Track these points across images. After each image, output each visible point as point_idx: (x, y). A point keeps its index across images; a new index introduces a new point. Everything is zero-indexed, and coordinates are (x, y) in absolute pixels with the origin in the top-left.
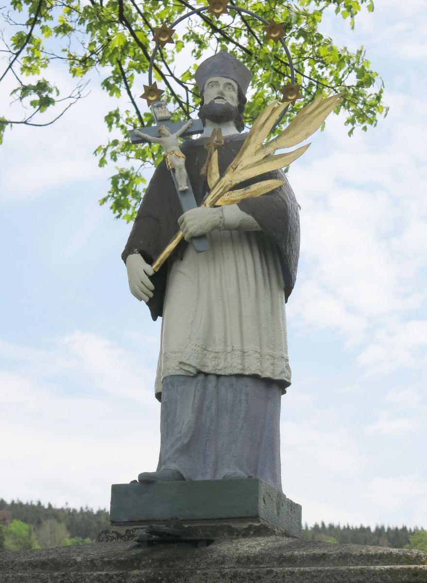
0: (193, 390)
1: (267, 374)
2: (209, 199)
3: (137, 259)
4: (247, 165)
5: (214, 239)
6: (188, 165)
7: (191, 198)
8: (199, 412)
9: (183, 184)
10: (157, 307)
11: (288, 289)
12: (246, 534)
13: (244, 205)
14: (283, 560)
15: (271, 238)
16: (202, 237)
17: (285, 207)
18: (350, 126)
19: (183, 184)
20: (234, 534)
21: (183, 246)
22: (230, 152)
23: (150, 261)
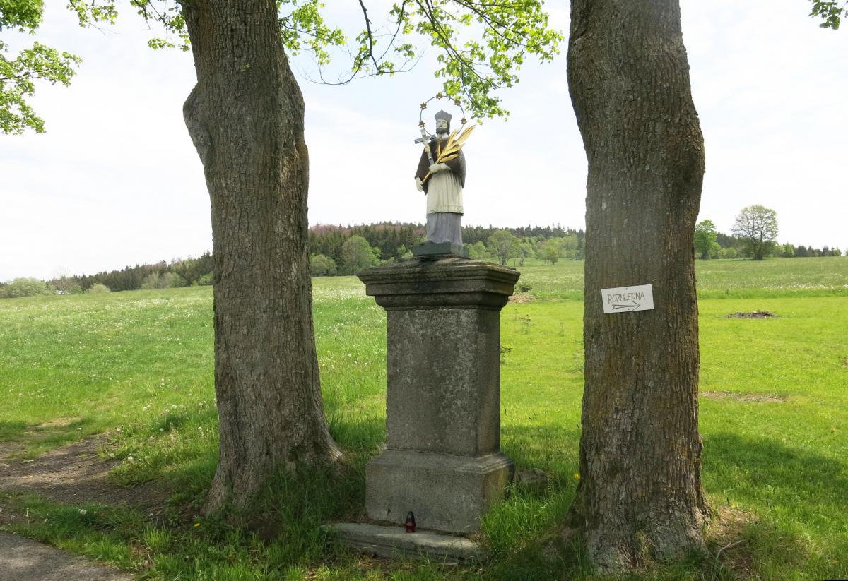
0: (435, 218)
1: (456, 212)
2: (438, 161)
3: (418, 179)
4: (449, 149)
5: (439, 173)
6: (431, 149)
7: (432, 161)
8: (437, 224)
9: (430, 157)
10: (425, 187)
11: (463, 185)
12: (447, 258)
13: (447, 163)
14: (453, 265)
15: (456, 170)
16: (435, 173)
17: (309, 365)
18: (542, 60)
19: (430, 157)
20: (445, 258)
21: (431, 176)
22: (444, 143)
23: (422, 180)
